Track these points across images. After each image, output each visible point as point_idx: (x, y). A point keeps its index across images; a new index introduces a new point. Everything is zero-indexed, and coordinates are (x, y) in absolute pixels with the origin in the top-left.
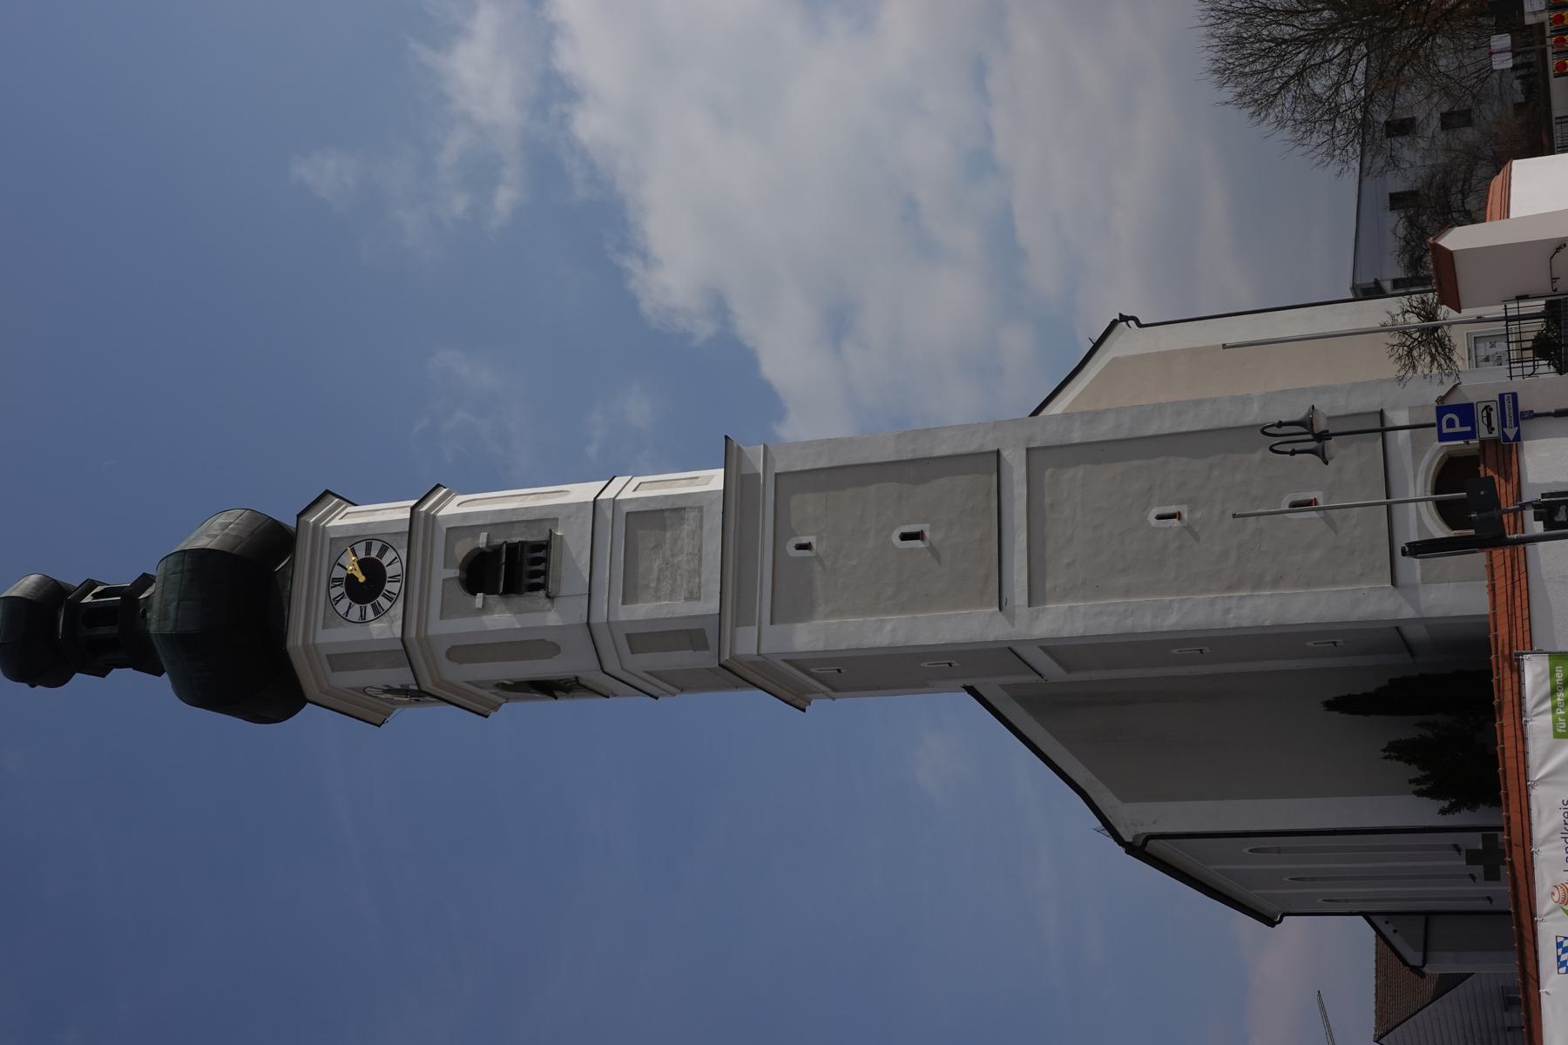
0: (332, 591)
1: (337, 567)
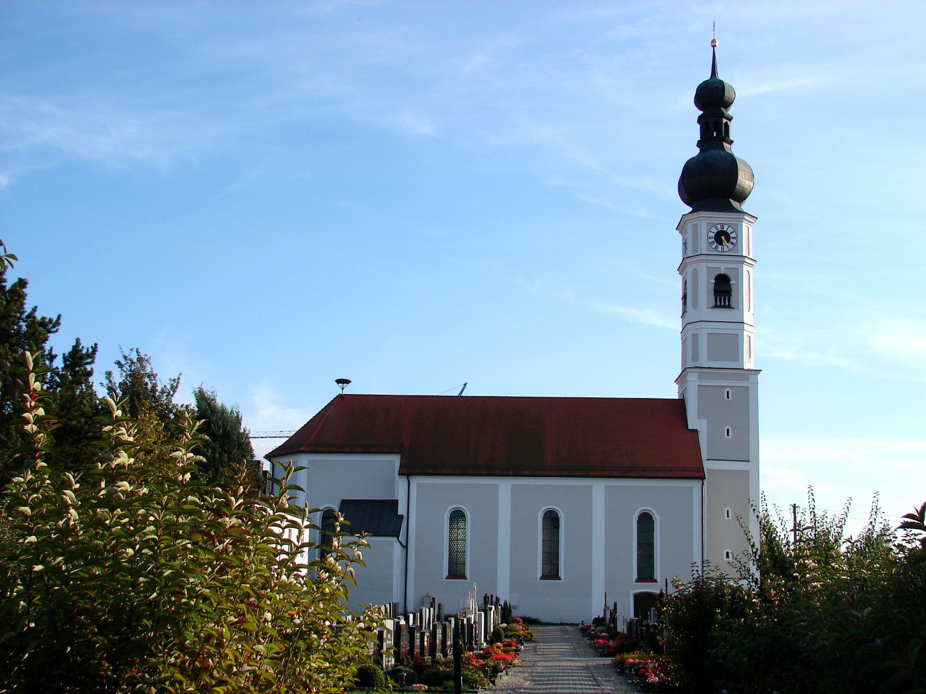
0: (719, 225)
1: (727, 226)
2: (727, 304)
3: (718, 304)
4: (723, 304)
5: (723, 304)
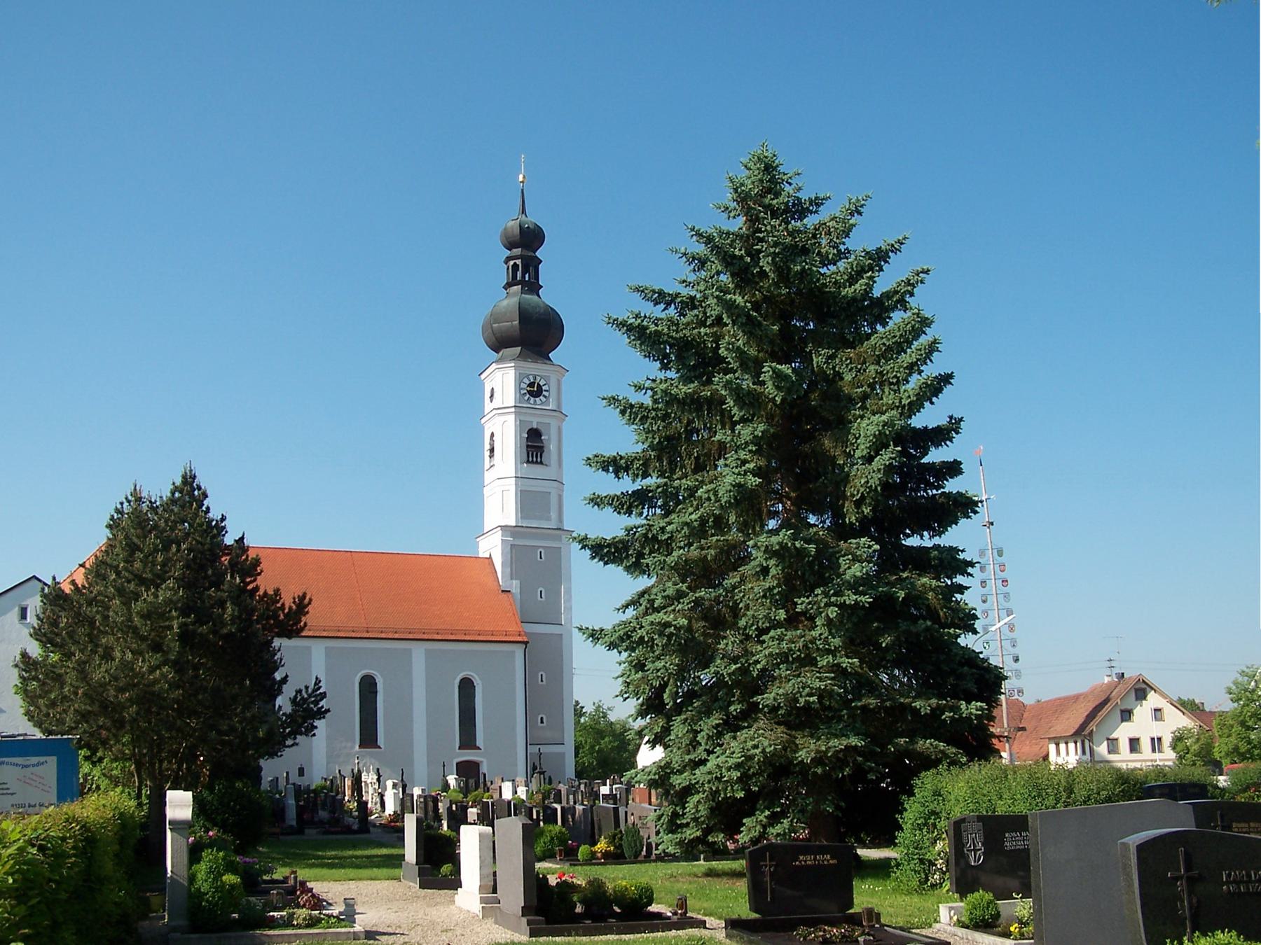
2: (539, 460)
3: (530, 459)
4: (535, 459)
5: (535, 459)
